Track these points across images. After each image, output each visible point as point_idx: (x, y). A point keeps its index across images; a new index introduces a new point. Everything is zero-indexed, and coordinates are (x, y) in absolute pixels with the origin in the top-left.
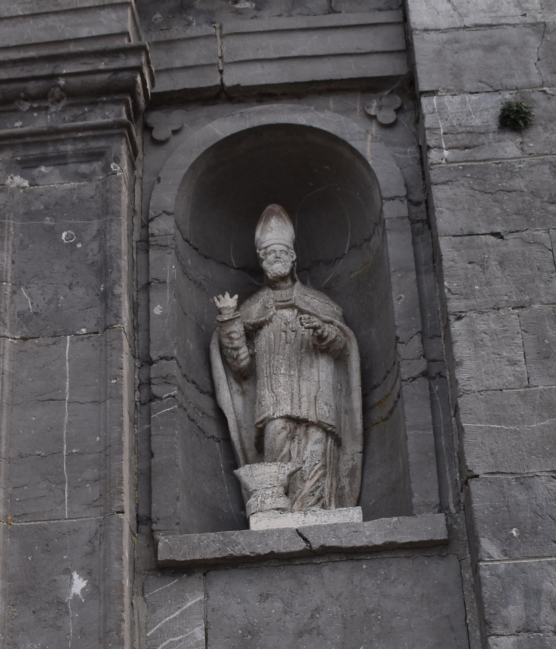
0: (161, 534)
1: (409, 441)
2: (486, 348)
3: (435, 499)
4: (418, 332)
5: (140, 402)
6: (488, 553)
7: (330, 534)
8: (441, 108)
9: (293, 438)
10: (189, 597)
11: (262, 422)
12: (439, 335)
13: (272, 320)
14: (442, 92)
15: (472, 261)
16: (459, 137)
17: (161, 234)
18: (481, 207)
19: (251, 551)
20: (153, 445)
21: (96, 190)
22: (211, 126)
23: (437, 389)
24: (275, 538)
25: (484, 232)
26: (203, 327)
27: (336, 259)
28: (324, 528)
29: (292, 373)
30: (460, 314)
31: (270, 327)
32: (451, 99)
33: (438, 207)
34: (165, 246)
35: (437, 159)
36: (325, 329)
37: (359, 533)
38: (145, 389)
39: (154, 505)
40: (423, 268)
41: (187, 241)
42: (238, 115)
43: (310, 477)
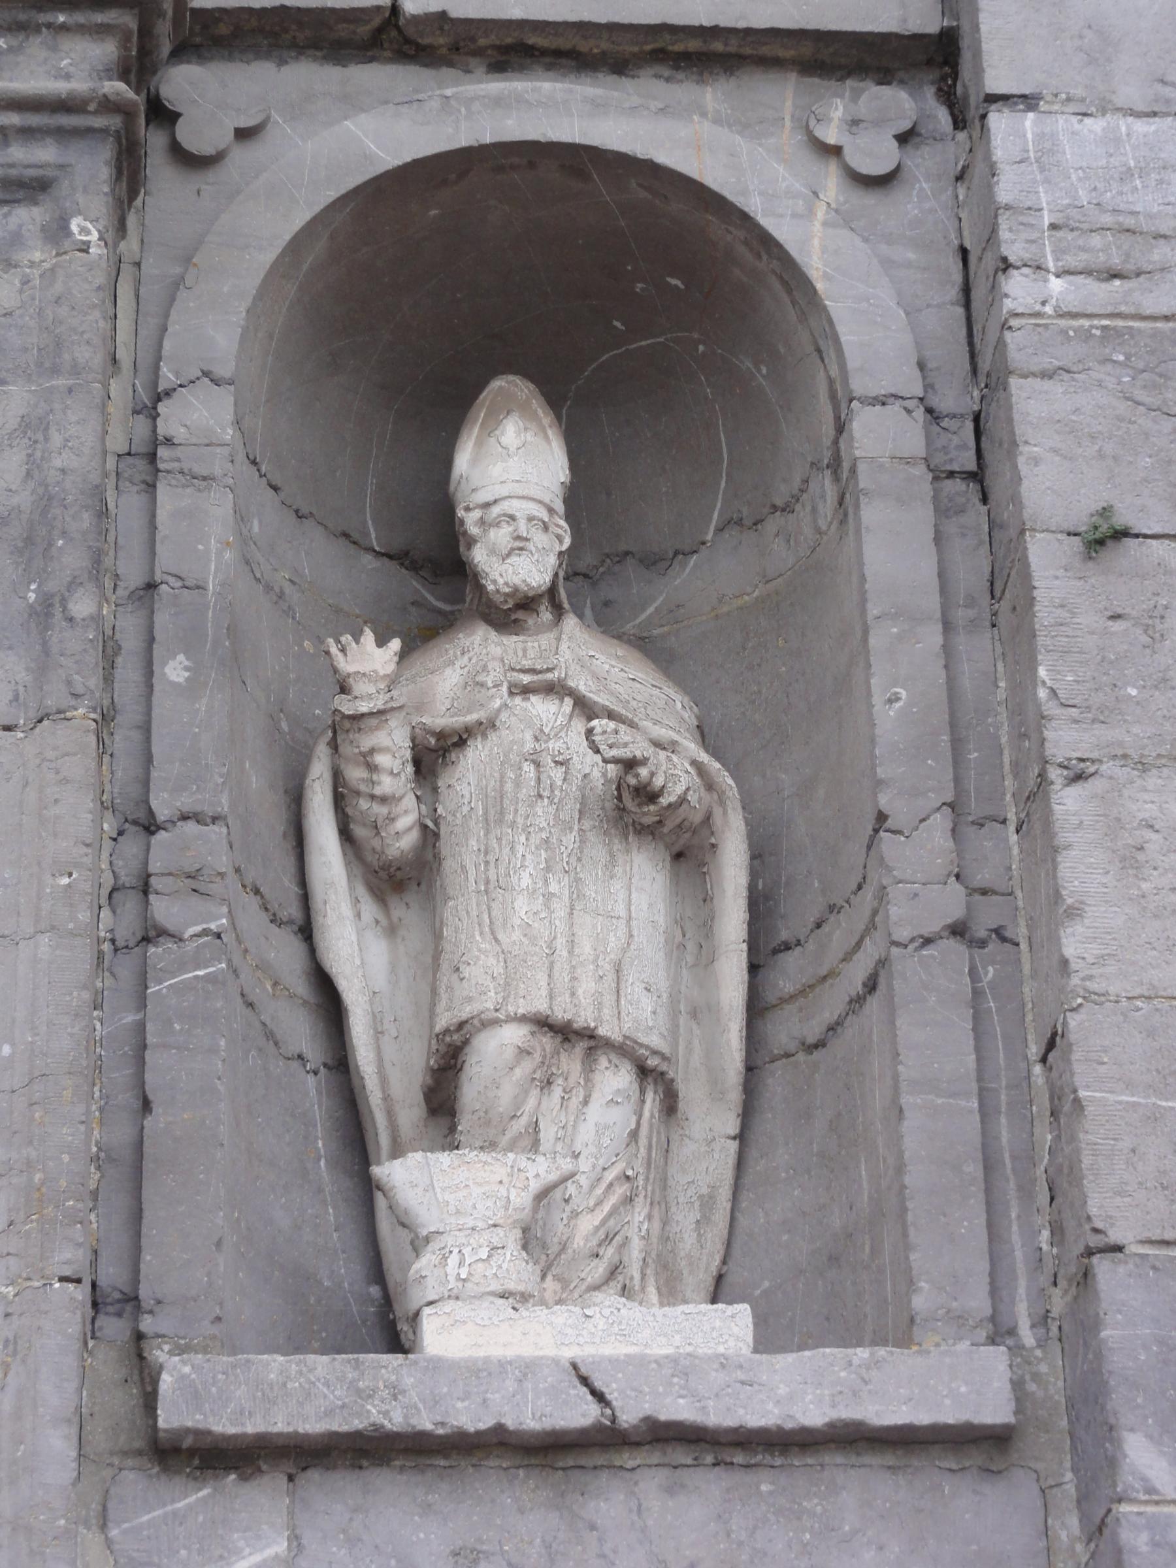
0: (166, 1348)
1: (906, 1123)
2: (1155, 873)
3: (978, 1302)
4: (944, 804)
5: (113, 941)
6: (1144, 1479)
7: (671, 1384)
8: (1048, 150)
9: (549, 1083)
10: (241, 1544)
11: (461, 1025)
12: (1001, 819)
13: (498, 724)
14: (1053, 103)
15: (1120, 611)
16: (1096, 240)
17: (194, 441)
18: (1150, 457)
19: (439, 1419)
20: (148, 1076)
21: (21, 291)
22: (353, 128)
23: (990, 975)
24: (510, 1385)
25: (1157, 529)
26: (284, 726)
27: (676, 553)
28: (654, 1366)
29: (553, 887)
30: (1082, 765)
31: (489, 743)
32: (1077, 127)
33: (1026, 442)
34: (205, 478)
35: (1030, 301)
36: (657, 766)
37: (756, 1387)
38: (128, 905)
39: (148, 1258)
40: (961, 615)
41: (254, 462)
42: (435, 104)
43: (592, 1203)
